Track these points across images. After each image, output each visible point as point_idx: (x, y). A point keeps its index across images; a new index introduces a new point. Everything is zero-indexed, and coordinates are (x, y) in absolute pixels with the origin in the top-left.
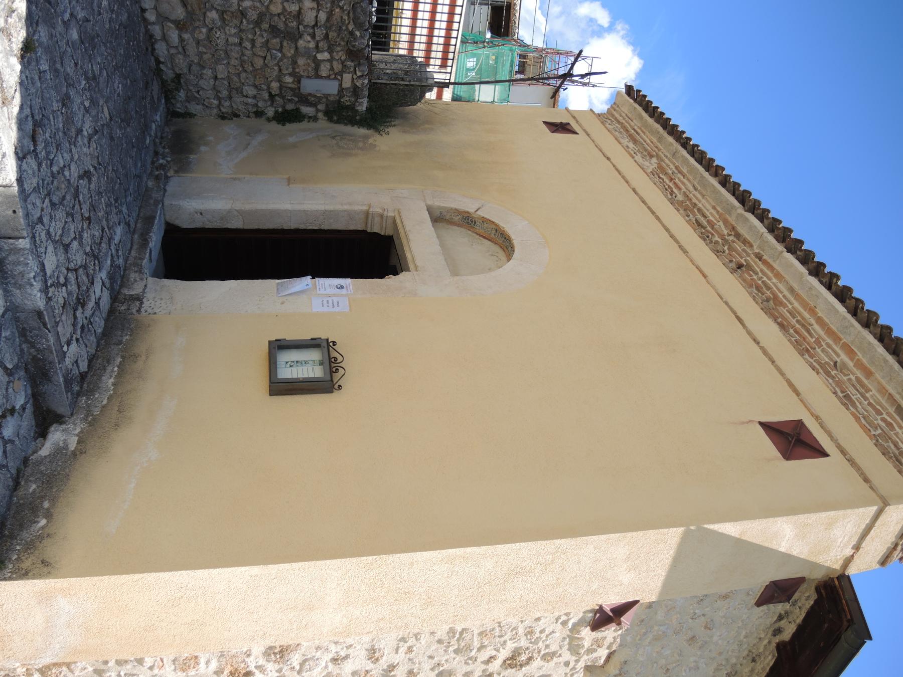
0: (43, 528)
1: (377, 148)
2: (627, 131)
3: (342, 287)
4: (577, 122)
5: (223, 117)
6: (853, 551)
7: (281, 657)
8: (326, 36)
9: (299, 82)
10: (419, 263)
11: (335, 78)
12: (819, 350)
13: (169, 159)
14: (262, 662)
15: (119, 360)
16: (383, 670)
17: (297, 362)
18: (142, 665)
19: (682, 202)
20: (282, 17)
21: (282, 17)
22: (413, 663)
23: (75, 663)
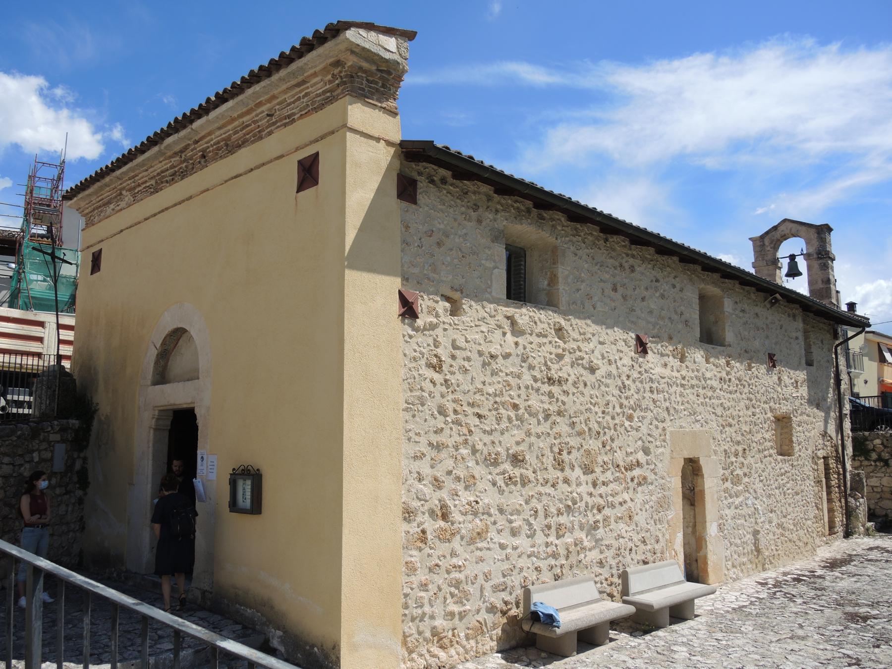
0: (318, 649)
1: (109, 414)
2: (100, 207)
3: (202, 458)
4: (92, 246)
5: (83, 528)
6: (381, 141)
7: (413, 513)
8: (21, 456)
9: (56, 473)
10: (190, 401)
11: (53, 446)
12: (260, 123)
13: (113, 569)
14: (415, 524)
15: (238, 606)
16: (432, 449)
17: (243, 495)
18: (409, 594)
19: (156, 182)
20: (7, 489)
21: (7, 489)
22: (428, 431)
23: (404, 633)
